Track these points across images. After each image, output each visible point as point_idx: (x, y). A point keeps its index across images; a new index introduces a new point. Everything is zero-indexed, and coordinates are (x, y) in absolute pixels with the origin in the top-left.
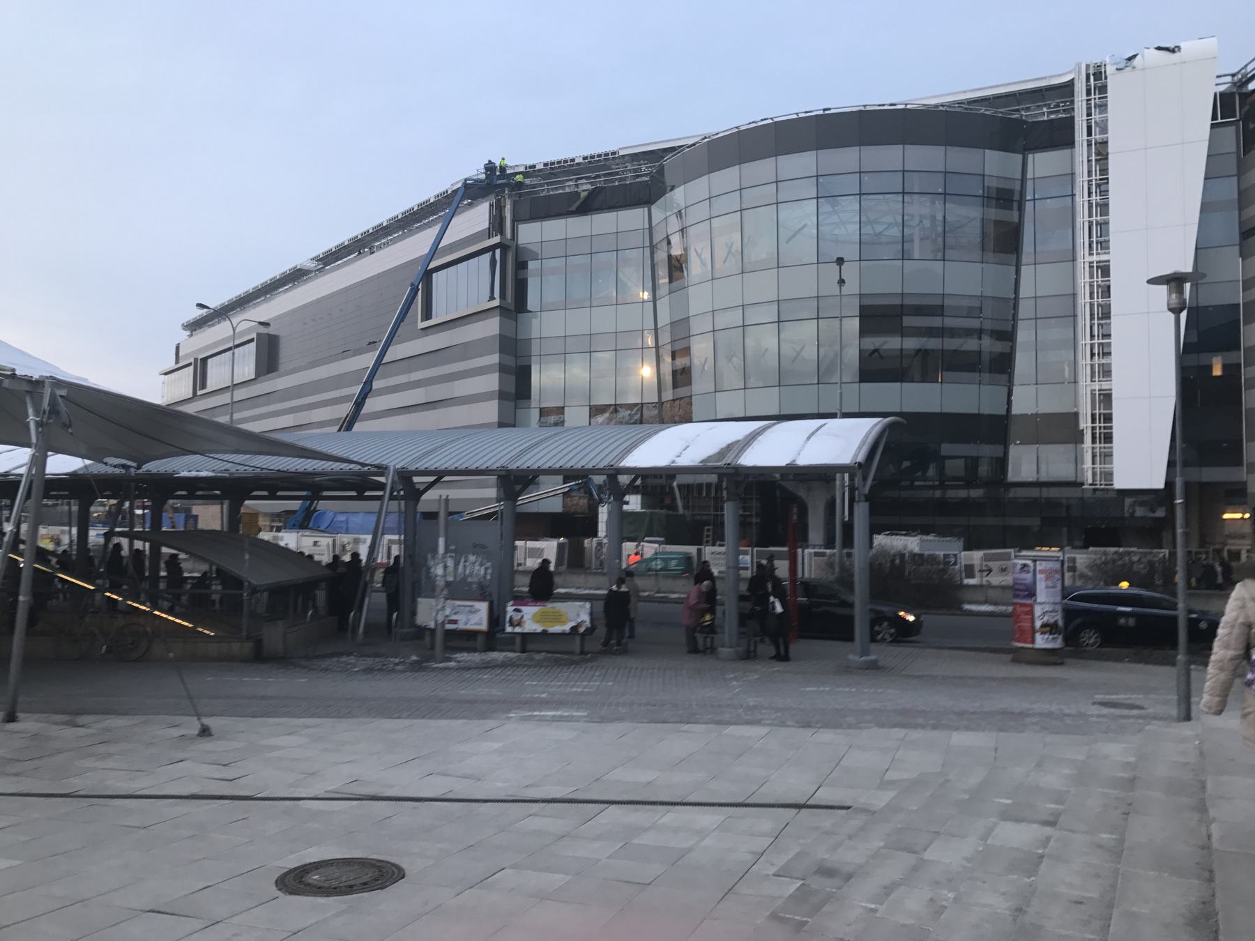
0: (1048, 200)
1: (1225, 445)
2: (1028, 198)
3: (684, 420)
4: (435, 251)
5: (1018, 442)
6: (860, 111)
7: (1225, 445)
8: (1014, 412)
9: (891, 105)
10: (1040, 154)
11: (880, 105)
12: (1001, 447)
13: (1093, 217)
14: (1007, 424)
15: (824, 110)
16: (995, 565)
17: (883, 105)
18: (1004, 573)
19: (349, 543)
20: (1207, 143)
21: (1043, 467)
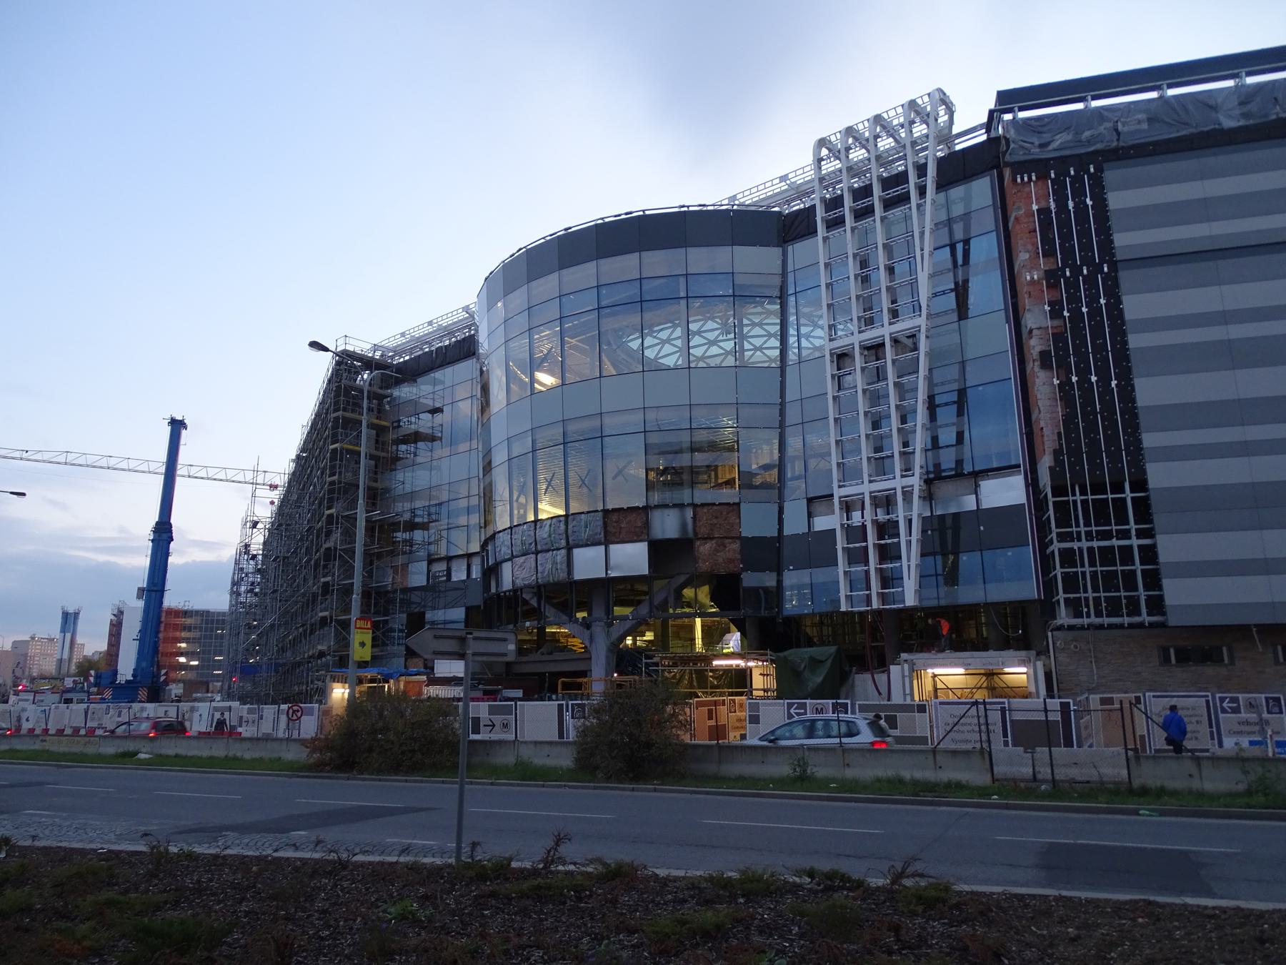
0: (809, 292)
1: (982, 528)
2: (790, 292)
3: (169, 534)
4: (592, 512)
5: (791, 568)
6: (596, 225)
7: (982, 528)
8: (786, 532)
9: (626, 214)
10: (798, 244)
11: (616, 216)
12: (774, 575)
13: (1138, 538)
14: (779, 547)
15: (566, 229)
16: (498, 719)
17: (619, 215)
18: (506, 730)
19: (187, 712)
20: (1274, 622)
21: (153, 467)
